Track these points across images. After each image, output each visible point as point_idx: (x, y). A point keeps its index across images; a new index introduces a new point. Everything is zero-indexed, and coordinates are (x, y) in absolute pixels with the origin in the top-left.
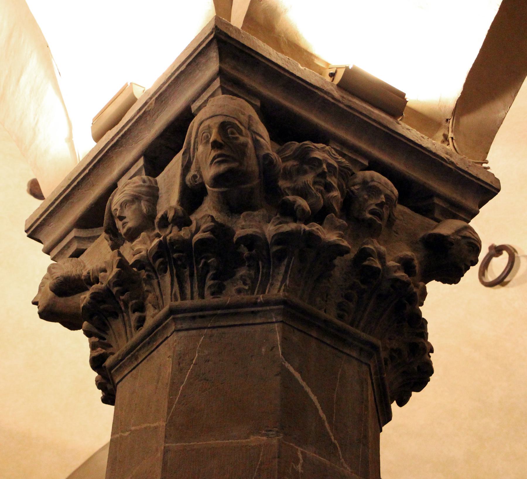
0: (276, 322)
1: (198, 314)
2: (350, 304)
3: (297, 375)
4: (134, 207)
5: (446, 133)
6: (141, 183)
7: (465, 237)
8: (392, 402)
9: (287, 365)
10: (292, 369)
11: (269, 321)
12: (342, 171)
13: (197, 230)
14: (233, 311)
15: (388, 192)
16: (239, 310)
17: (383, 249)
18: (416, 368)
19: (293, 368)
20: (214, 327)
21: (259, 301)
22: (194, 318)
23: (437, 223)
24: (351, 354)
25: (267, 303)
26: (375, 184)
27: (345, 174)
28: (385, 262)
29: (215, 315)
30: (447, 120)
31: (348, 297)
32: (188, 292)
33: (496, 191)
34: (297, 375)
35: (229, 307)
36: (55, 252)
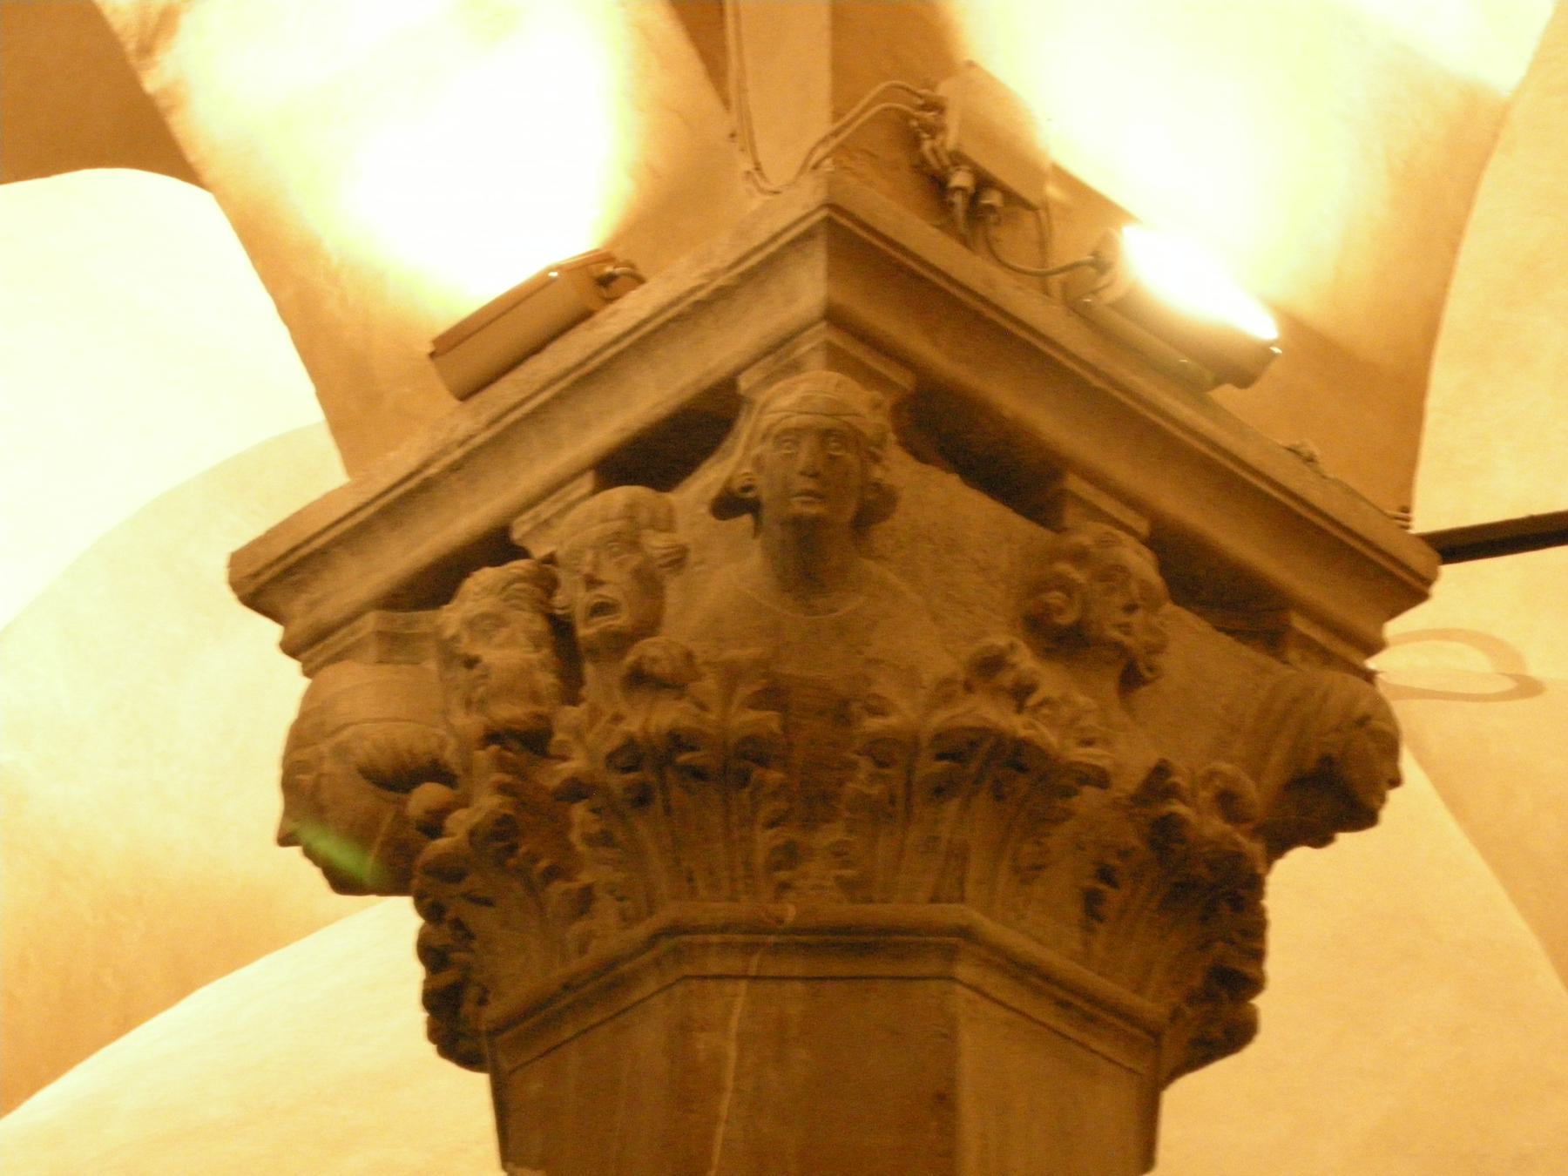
15: (596, 531)
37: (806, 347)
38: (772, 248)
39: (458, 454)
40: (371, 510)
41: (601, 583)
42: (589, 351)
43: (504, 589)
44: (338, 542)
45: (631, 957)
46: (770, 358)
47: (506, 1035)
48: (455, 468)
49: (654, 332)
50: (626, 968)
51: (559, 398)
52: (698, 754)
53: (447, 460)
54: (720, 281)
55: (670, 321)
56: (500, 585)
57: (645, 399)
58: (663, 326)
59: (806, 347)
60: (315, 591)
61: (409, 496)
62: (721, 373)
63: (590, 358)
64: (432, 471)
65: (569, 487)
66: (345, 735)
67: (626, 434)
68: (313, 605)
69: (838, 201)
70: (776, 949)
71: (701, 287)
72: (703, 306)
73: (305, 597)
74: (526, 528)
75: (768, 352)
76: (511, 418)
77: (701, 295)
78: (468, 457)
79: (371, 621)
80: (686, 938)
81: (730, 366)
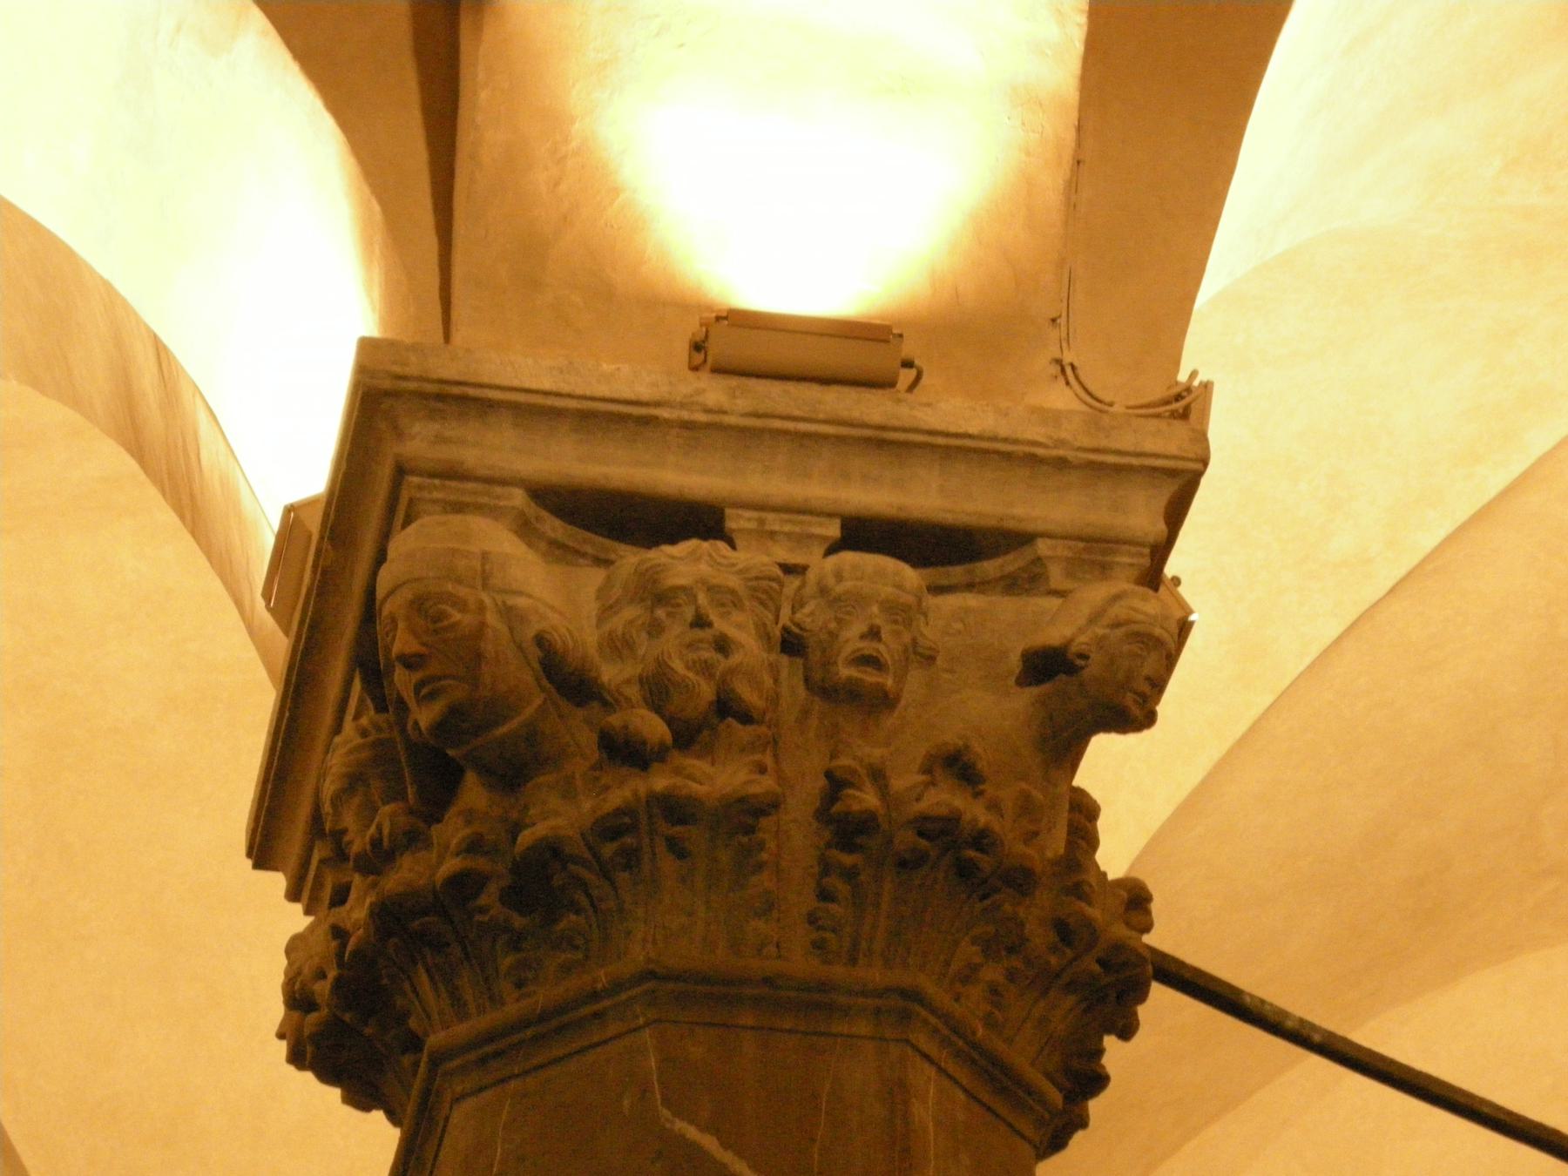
0: (647, 1025)
1: (489, 1049)
2: (833, 907)
3: (709, 1142)
4: (356, 800)
5: (1058, 355)
6: (360, 740)
7: (1117, 625)
8: (1100, 1052)
9: (681, 1126)
10: (692, 1133)
11: (633, 1026)
12: (755, 589)
13: (441, 859)
14: (552, 1025)
15: (887, 591)
16: (565, 1018)
17: (876, 753)
18: (1097, 968)
19: (698, 1126)
20: (527, 1072)
21: (599, 986)
22: (483, 1061)
23: (1060, 601)
24: (854, 1030)
25: (618, 986)
26: (848, 584)
27: (765, 592)
28: (886, 786)
29: (521, 1042)
30: (1054, 320)
31: (825, 895)
32: (468, 995)
33: (1199, 466)
34: (709, 1142)
35: (543, 1018)
36: (306, 894)
37: (1126, 560)
38: (1135, 461)
39: (702, 417)
40: (573, 404)
41: (880, 640)
42: (896, 423)
43: (757, 578)
44: (515, 407)
45: (933, 1011)
46: (1081, 545)
47: (671, 986)
48: (688, 426)
49: (974, 450)
50: (842, 999)
51: (840, 440)
52: (986, 858)
53: (685, 415)
54: (1070, 455)
55: (998, 452)
56: (753, 574)
57: (924, 496)
58: (986, 452)
59: (1126, 560)
60: (453, 429)
61: (622, 418)
62: (1030, 527)
63: (895, 429)
64: (664, 413)
65: (814, 519)
66: (521, 602)
67: (903, 515)
68: (440, 439)
69: (888, 392)
70: (958, 1054)
71: (1045, 446)
72: (1033, 461)
73: (434, 427)
74: (744, 524)
75: (1080, 538)
76: (777, 424)
77: (1040, 451)
78: (708, 426)
79: (518, 498)
80: (918, 1008)
81: (1040, 527)
